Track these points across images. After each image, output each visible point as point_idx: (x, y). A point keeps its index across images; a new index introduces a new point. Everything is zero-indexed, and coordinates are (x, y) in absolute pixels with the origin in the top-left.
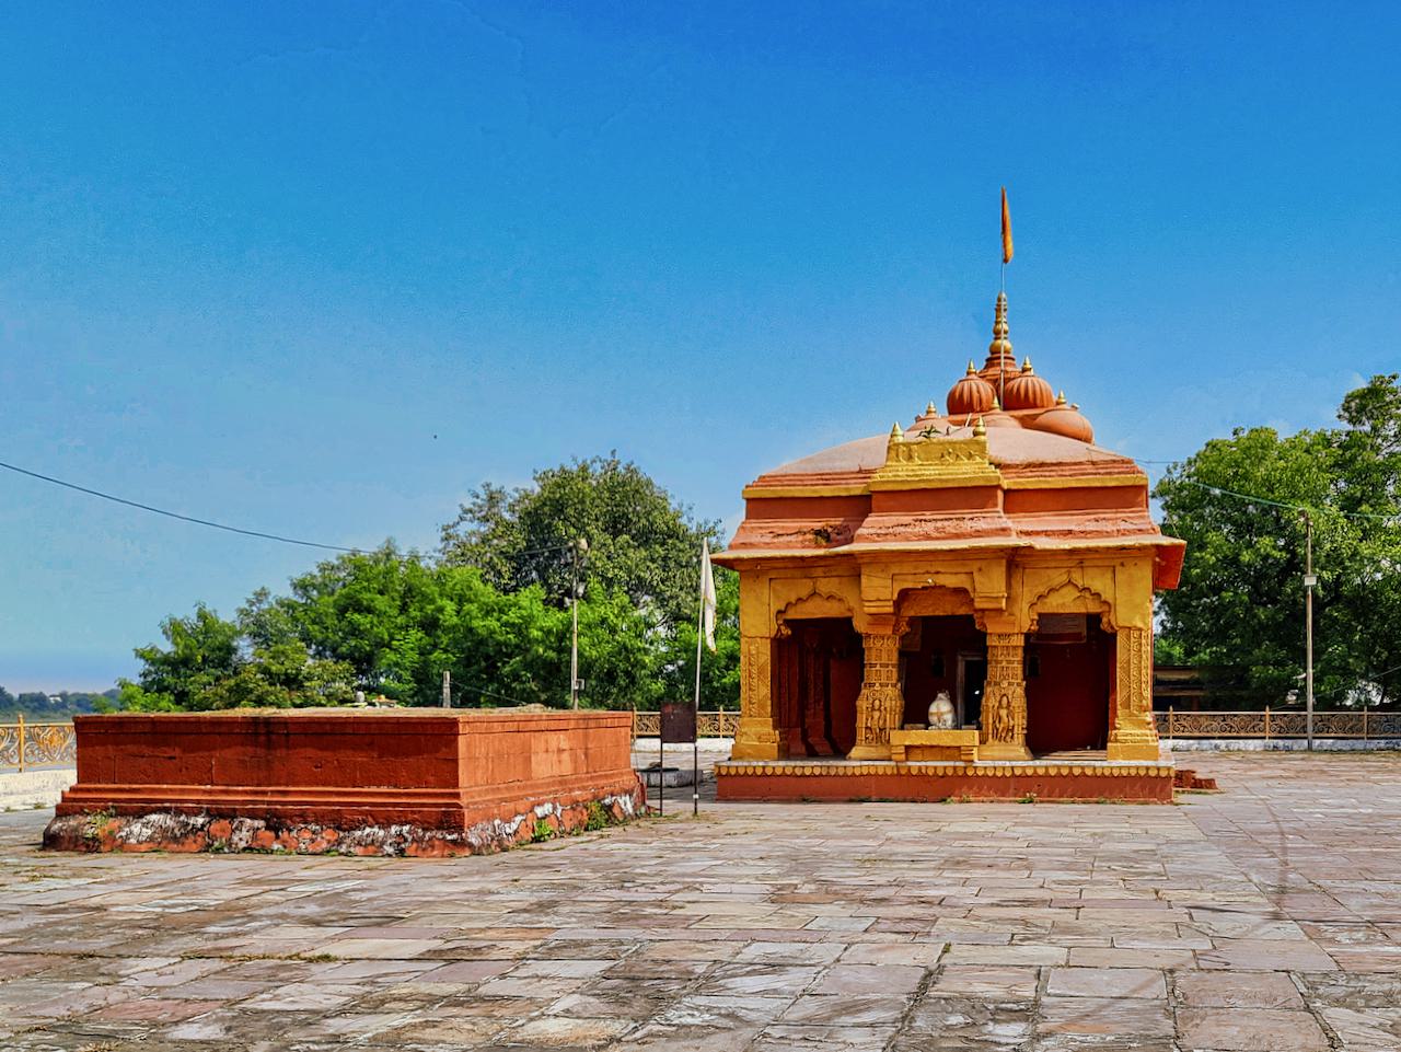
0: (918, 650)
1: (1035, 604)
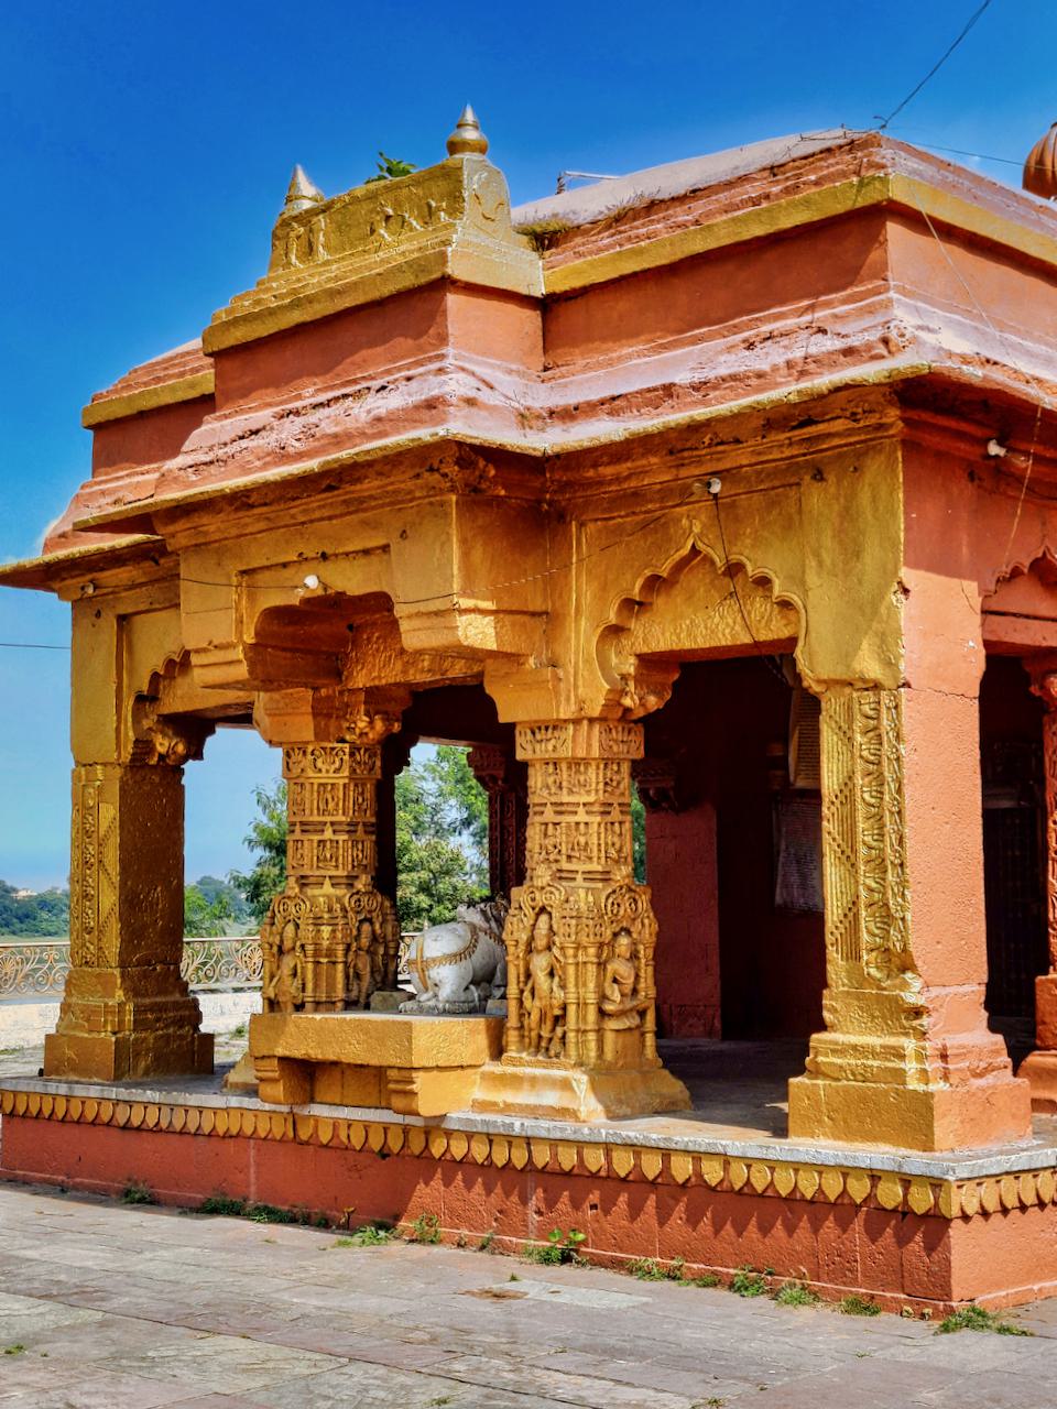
1: (990, 596)
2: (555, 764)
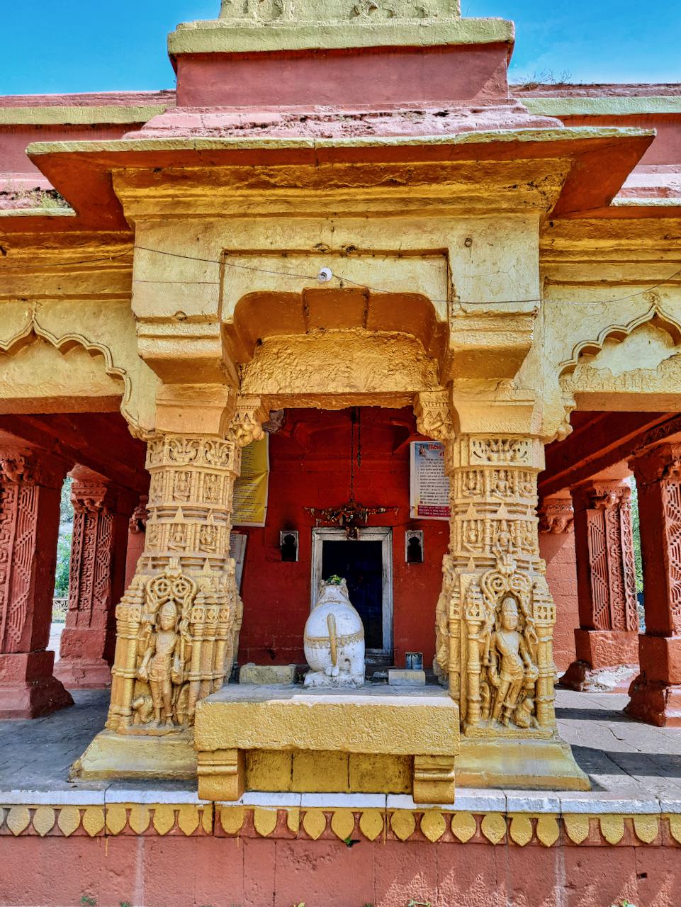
0: (263, 525)
2: (506, 472)
